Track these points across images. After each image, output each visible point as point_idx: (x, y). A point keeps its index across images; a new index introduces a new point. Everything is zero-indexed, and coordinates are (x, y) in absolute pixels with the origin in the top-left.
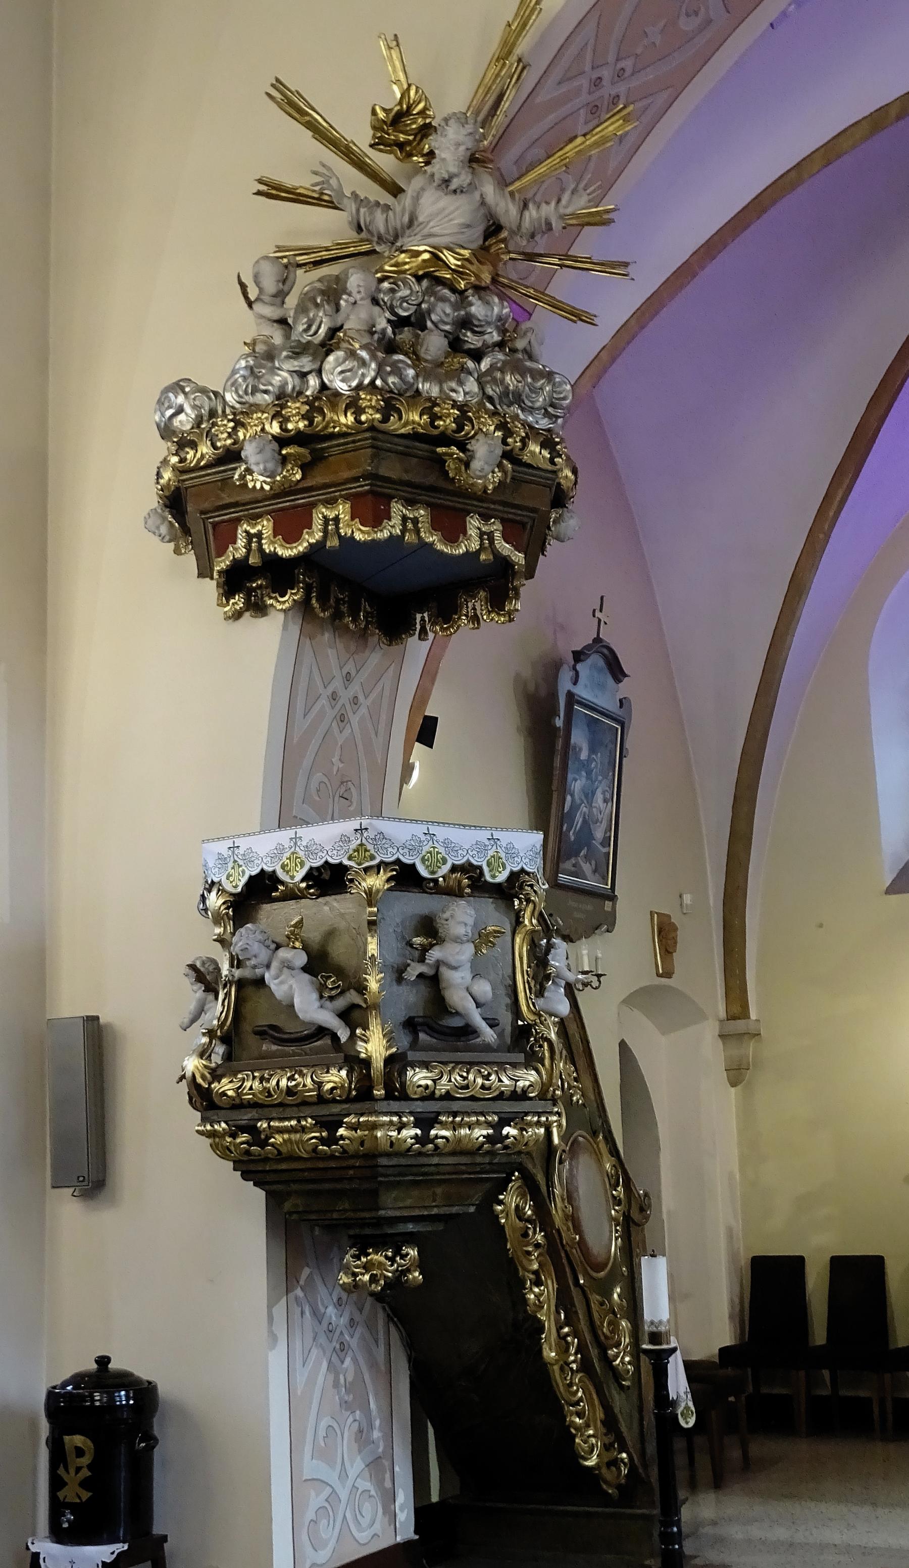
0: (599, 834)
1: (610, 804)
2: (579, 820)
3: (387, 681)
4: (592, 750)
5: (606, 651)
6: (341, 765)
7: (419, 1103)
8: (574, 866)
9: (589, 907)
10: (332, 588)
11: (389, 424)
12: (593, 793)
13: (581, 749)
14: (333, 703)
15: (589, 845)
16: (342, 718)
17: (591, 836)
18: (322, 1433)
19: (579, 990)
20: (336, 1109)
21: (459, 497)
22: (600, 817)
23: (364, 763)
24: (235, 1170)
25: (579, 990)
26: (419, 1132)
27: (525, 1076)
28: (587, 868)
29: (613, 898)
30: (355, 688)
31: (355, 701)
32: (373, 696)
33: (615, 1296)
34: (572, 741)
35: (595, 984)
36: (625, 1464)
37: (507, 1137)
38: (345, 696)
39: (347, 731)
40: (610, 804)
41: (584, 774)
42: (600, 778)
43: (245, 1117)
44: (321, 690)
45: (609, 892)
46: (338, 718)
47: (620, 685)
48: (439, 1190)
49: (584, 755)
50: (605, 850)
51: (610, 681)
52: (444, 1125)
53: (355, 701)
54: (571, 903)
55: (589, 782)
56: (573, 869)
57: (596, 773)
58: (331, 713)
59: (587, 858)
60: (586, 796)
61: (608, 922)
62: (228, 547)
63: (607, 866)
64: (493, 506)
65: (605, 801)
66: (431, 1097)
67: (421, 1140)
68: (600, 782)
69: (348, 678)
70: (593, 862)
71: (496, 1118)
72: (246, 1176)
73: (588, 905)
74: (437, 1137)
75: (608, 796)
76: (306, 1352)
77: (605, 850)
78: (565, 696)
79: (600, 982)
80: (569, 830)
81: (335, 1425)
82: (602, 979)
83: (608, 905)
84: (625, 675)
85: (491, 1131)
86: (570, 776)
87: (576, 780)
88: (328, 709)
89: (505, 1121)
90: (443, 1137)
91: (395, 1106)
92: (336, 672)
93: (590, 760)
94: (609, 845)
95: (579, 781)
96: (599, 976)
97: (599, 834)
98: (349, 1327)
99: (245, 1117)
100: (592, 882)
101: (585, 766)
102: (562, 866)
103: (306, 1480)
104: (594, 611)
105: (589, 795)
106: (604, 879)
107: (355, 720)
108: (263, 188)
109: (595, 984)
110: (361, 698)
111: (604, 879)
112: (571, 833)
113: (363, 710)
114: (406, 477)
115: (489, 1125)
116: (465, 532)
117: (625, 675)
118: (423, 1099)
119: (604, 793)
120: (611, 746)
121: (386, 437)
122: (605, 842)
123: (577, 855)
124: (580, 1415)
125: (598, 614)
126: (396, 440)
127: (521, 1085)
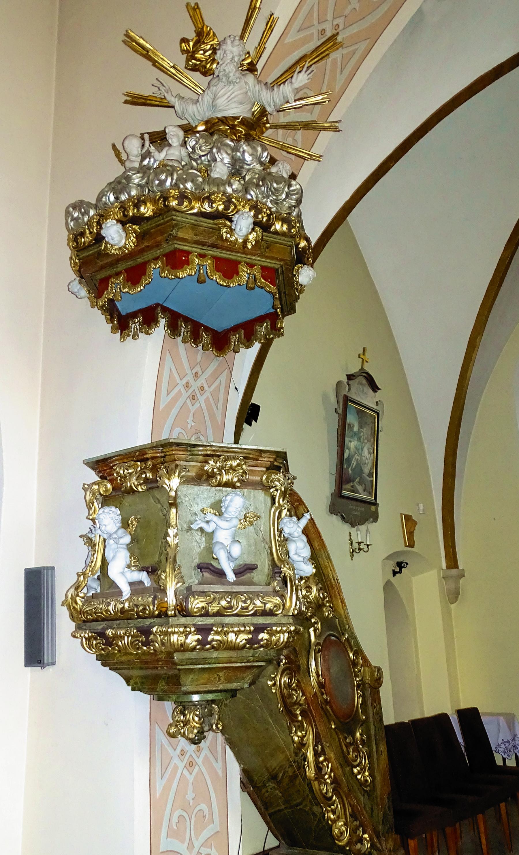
0: (366, 470)
1: (372, 455)
2: (354, 463)
3: (223, 378)
4: (361, 427)
5: (365, 374)
6: (193, 424)
7: (199, 618)
8: (352, 487)
9: (363, 509)
10: (179, 323)
11: (183, 207)
12: (362, 449)
13: (354, 426)
14: (187, 389)
15: (360, 476)
16: (193, 398)
17: (362, 471)
18: (175, 820)
19: (357, 552)
20: (148, 622)
21: (230, 251)
22: (367, 462)
23: (209, 423)
24: (97, 660)
25: (357, 552)
26: (200, 637)
27: (272, 600)
28: (360, 488)
29: (376, 504)
30: (202, 381)
31: (202, 388)
32: (213, 387)
33: (358, 735)
34: (348, 421)
35: (366, 549)
36: (368, 841)
37: (262, 640)
38: (195, 386)
39: (197, 405)
40: (372, 455)
41: (356, 438)
42: (366, 441)
43: (99, 626)
44: (178, 381)
45: (374, 501)
46: (191, 397)
47: (376, 393)
48: (221, 674)
49: (356, 429)
50: (371, 479)
51: (370, 391)
52: (217, 633)
53: (202, 388)
54: (351, 507)
55: (359, 443)
56: (352, 488)
57: (363, 439)
58: (185, 395)
59: (360, 483)
60: (358, 450)
61: (375, 518)
62: (104, 292)
63: (372, 487)
64: (254, 258)
65: (370, 453)
66: (207, 614)
67: (202, 643)
68: (366, 443)
69: (196, 375)
70: (364, 485)
71: (252, 628)
72: (104, 665)
73: (361, 508)
74: (213, 640)
75: (371, 451)
76: (163, 771)
77: (371, 479)
78: (342, 398)
79: (368, 549)
80: (348, 467)
81: (185, 814)
82: (370, 547)
83: (373, 508)
84: (379, 389)
85: (250, 636)
86: (347, 440)
87: (351, 442)
88: (183, 391)
89: (259, 629)
90: (216, 641)
91: (183, 620)
92: (188, 371)
93: (359, 432)
94: (373, 477)
95: (353, 442)
96: (368, 545)
97: (366, 470)
98: (196, 751)
99: (99, 626)
100: (363, 496)
101: (357, 435)
102: (344, 487)
103: (162, 852)
104: (359, 355)
105: (359, 450)
106: (370, 494)
107: (202, 399)
108: (129, 98)
109: (366, 549)
110: (206, 387)
111: (370, 494)
112: (350, 469)
113: (208, 394)
114: (195, 238)
115: (249, 632)
116: (237, 273)
117: (379, 389)
118: (201, 616)
119: (368, 449)
120: (371, 425)
121: (181, 215)
122: (370, 475)
123: (353, 481)
124: (334, 812)
125: (362, 356)
126: (189, 217)
127: (269, 607)
